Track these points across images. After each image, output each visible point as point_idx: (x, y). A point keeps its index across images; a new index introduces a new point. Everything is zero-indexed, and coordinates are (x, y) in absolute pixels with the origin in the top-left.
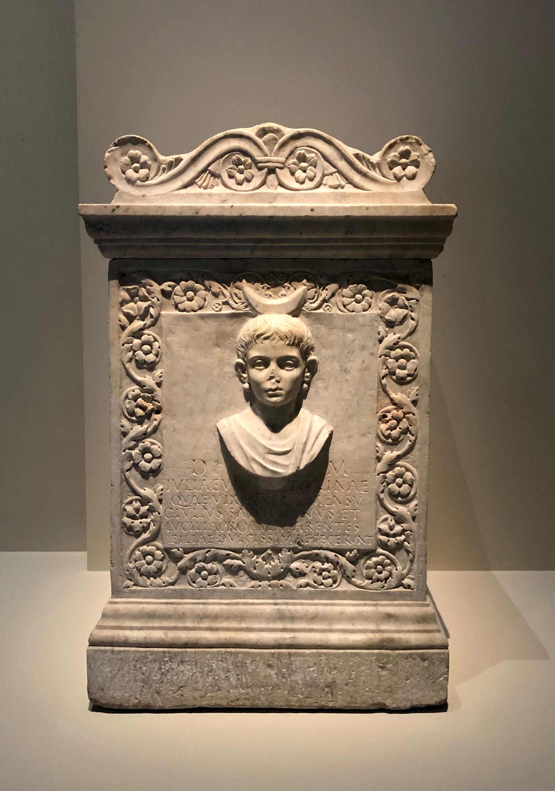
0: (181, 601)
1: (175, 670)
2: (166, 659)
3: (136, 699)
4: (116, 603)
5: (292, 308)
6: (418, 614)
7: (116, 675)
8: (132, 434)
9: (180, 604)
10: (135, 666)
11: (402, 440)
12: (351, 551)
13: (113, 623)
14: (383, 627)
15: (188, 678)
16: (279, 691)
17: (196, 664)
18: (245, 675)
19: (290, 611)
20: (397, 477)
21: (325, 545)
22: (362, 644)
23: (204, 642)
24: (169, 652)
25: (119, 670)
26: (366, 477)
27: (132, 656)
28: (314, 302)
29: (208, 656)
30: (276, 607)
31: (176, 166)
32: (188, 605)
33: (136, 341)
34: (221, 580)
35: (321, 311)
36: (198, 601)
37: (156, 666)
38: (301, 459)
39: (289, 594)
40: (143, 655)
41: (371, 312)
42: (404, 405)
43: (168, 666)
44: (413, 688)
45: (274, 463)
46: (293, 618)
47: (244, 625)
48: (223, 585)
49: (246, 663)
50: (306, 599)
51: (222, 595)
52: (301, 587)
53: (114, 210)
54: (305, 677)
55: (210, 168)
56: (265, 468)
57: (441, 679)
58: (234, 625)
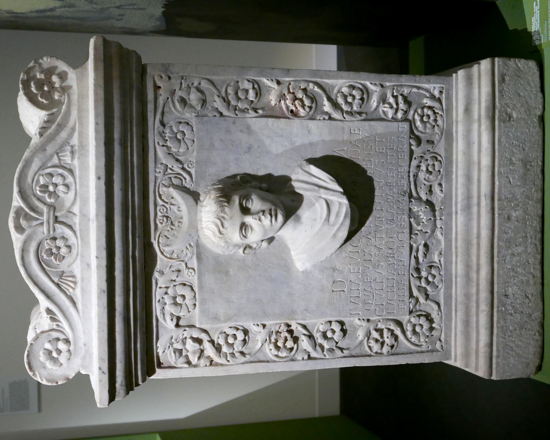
0: (454, 298)
1: (513, 301)
2: (503, 309)
3: (535, 335)
4: (456, 356)
5: (191, 200)
6: (464, 84)
7: (516, 352)
8: (310, 349)
9: (456, 299)
10: (509, 336)
11: (313, 95)
12: (411, 145)
13: (473, 358)
14: (476, 116)
15: (519, 289)
16: (529, 208)
17: (507, 282)
18: (516, 239)
19: (463, 200)
20: (346, 102)
21: (407, 169)
22: (491, 135)
23: (489, 277)
24: (498, 307)
25: (513, 350)
26: (347, 130)
27: (501, 339)
28: (185, 179)
29: (501, 272)
30: (459, 212)
31: (55, 314)
32: (458, 291)
33: (225, 349)
34: (436, 263)
35: (193, 171)
36: (454, 283)
37: (509, 317)
38: (333, 191)
39: (448, 199)
40: (500, 329)
41: (194, 123)
42: (281, 92)
43: (509, 308)
44: (526, 91)
45: (338, 215)
46: (468, 197)
47: (475, 241)
48: (440, 261)
49: (507, 239)
50: (452, 185)
51: (448, 262)
52: (442, 190)
53: (103, 372)
54: (517, 185)
55: (56, 280)
56: (342, 224)
57: (519, 65)
58: (474, 250)
